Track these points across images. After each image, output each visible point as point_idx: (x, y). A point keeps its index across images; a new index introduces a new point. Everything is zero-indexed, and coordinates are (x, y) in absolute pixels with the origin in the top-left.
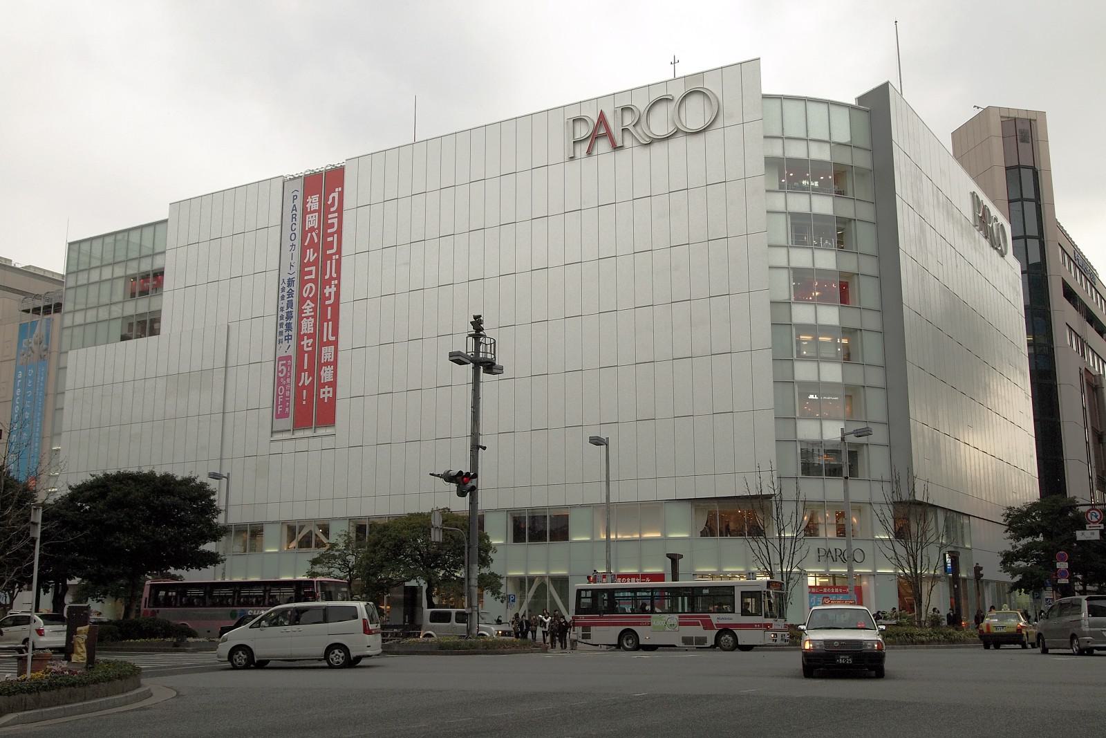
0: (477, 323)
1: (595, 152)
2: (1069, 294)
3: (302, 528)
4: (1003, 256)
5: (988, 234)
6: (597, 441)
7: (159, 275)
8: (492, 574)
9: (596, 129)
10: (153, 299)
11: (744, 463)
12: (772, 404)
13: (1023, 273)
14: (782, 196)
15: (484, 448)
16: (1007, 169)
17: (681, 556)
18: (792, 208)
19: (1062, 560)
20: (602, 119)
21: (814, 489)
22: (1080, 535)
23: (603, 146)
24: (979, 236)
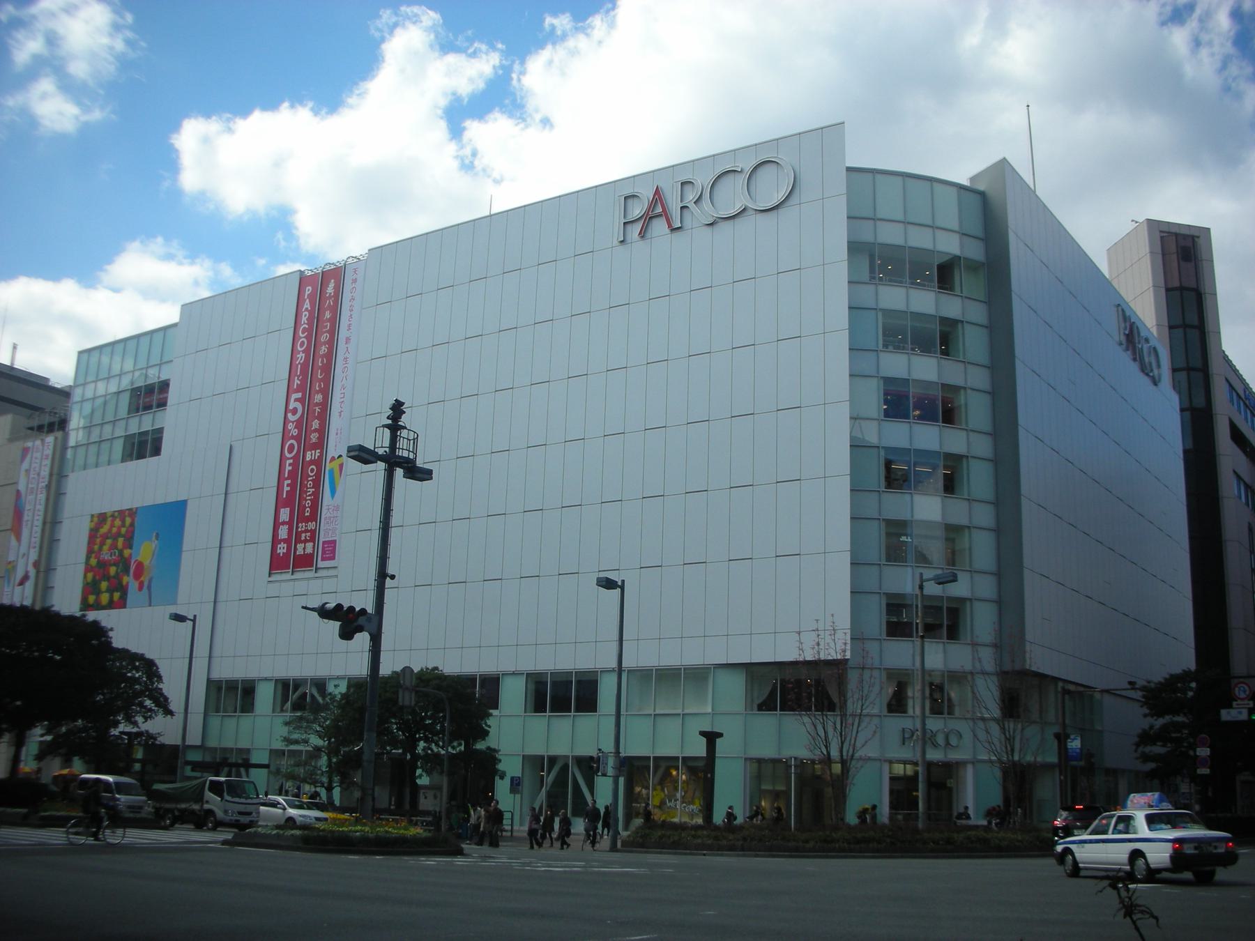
0: (398, 409)
1: (648, 235)
2: (1238, 437)
3: (296, 687)
5: (1137, 357)
6: (608, 584)
7: (164, 386)
8: (489, 748)
9: (653, 205)
10: (159, 415)
11: (812, 614)
13: (1182, 410)
14: (872, 288)
15: (393, 577)
16: (1168, 290)
17: (720, 735)
19: (1204, 745)
20: (658, 194)
21: (901, 654)
22: (1226, 715)
23: (659, 226)
24: (1126, 357)
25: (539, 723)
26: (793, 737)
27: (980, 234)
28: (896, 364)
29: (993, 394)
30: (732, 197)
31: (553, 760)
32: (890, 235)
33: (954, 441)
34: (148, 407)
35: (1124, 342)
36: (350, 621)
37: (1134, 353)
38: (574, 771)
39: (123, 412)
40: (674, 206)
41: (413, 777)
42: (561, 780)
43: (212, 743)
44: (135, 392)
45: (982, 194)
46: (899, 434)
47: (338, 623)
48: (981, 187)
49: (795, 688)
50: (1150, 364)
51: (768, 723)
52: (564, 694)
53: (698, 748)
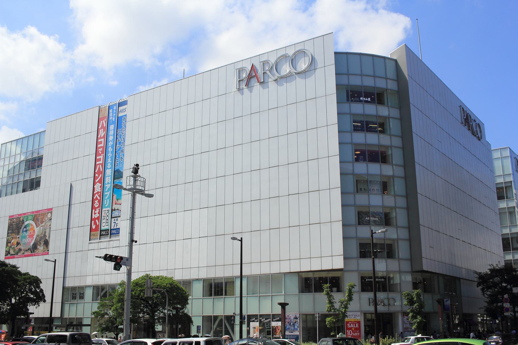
4: (480, 140)
7: (40, 159)
12: (342, 253)
15: (136, 242)
17: (288, 304)
18: (358, 203)
23: (254, 81)
24: (465, 129)
25: (209, 302)
26: (318, 303)
27: (395, 78)
28: (360, 138)
29: (403, 148)
30: (286, 69)
31: (216, 317)
32: (355, 81)
33: (387, 170)
34: (33, 168)
35: (464, 122)
36: (118, 262)
37: (469, 127)
38: (225, 322)
39: (22, 171)
40: (260, 72)
41: (153, 328)
42: (220, 324)
43: (66, 316)
44: (27, 161)
45: (396, 61)
46: (361, 168)
47: (114, 263)
48: (395, 58)
49: (312, 283)
50: (477, 131)
51: (308, 297)
52: (217, 288)
53: (278, 310)
